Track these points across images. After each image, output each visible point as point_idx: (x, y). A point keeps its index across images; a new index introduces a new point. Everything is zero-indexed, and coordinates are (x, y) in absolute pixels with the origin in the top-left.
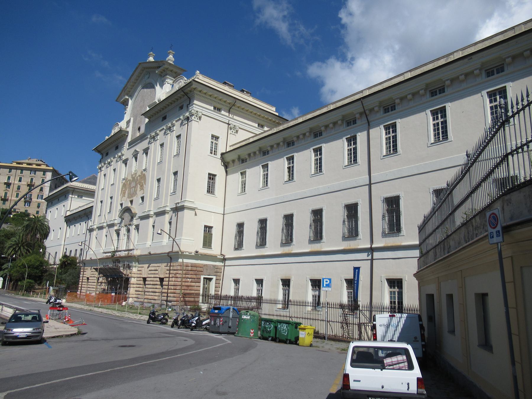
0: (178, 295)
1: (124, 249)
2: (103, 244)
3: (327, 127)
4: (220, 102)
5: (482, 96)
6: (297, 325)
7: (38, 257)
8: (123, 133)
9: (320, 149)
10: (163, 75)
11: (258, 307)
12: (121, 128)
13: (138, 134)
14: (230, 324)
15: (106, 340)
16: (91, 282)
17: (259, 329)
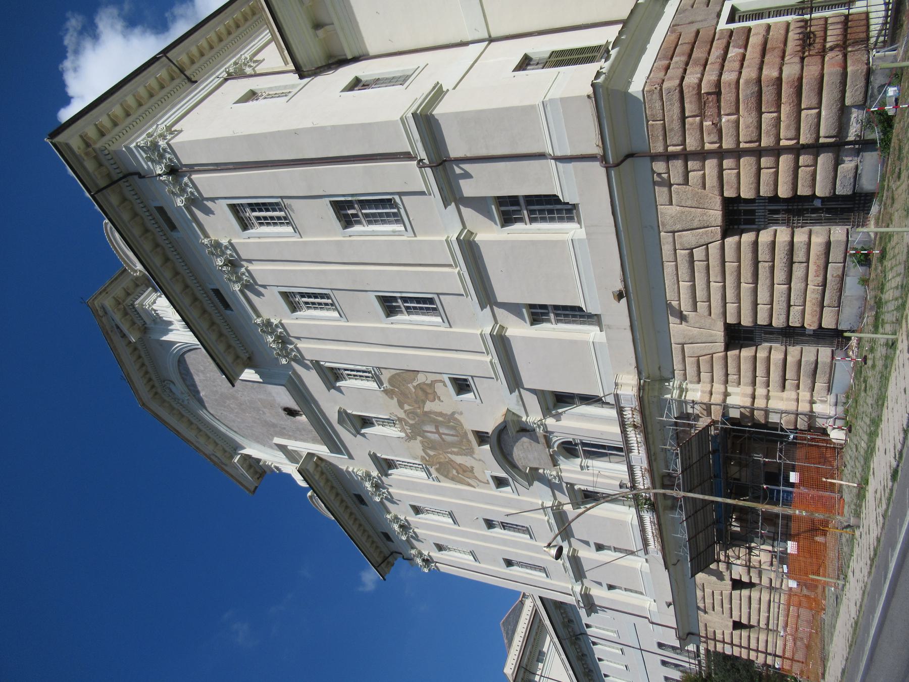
8: (311, 468)
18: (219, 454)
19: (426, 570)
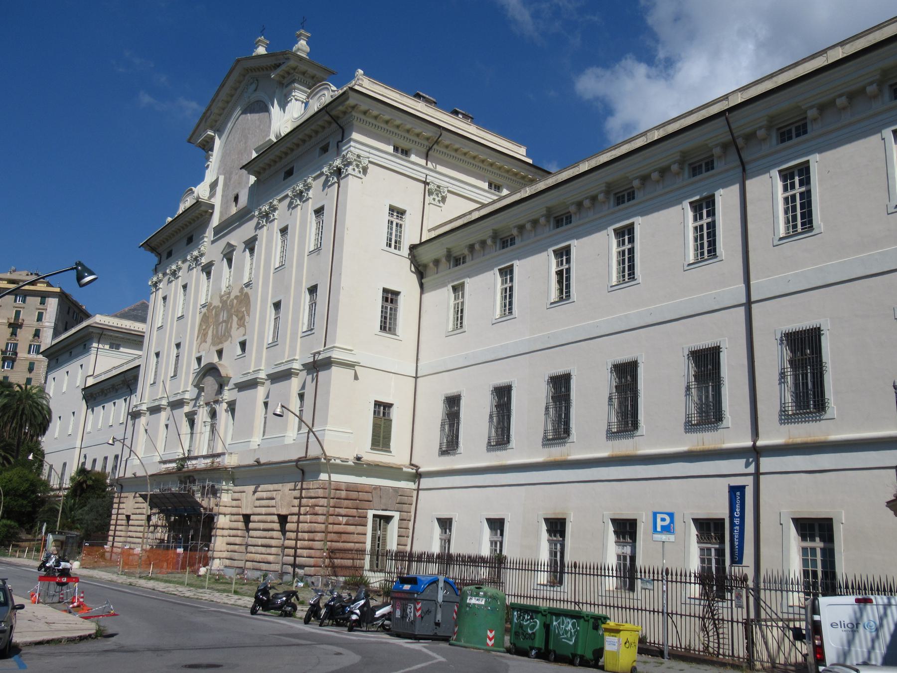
0: (318, 553)
1: (205, 453)
2: (160, 445)
3: (645, 179)
4: (407, 135)
5: (883, 139)
6: (598, 621)
7: (26, 472)
8: (203, 208)
9: (630, 229)
10: (285, 81)
11: (497, 581)
12: (198, 197)
13: (234, 210)
14: (439, 617)
15: (156, 650)
16: (135, 525)
17: (507, 631)
18: (212, 117)
19: (150, 283)
